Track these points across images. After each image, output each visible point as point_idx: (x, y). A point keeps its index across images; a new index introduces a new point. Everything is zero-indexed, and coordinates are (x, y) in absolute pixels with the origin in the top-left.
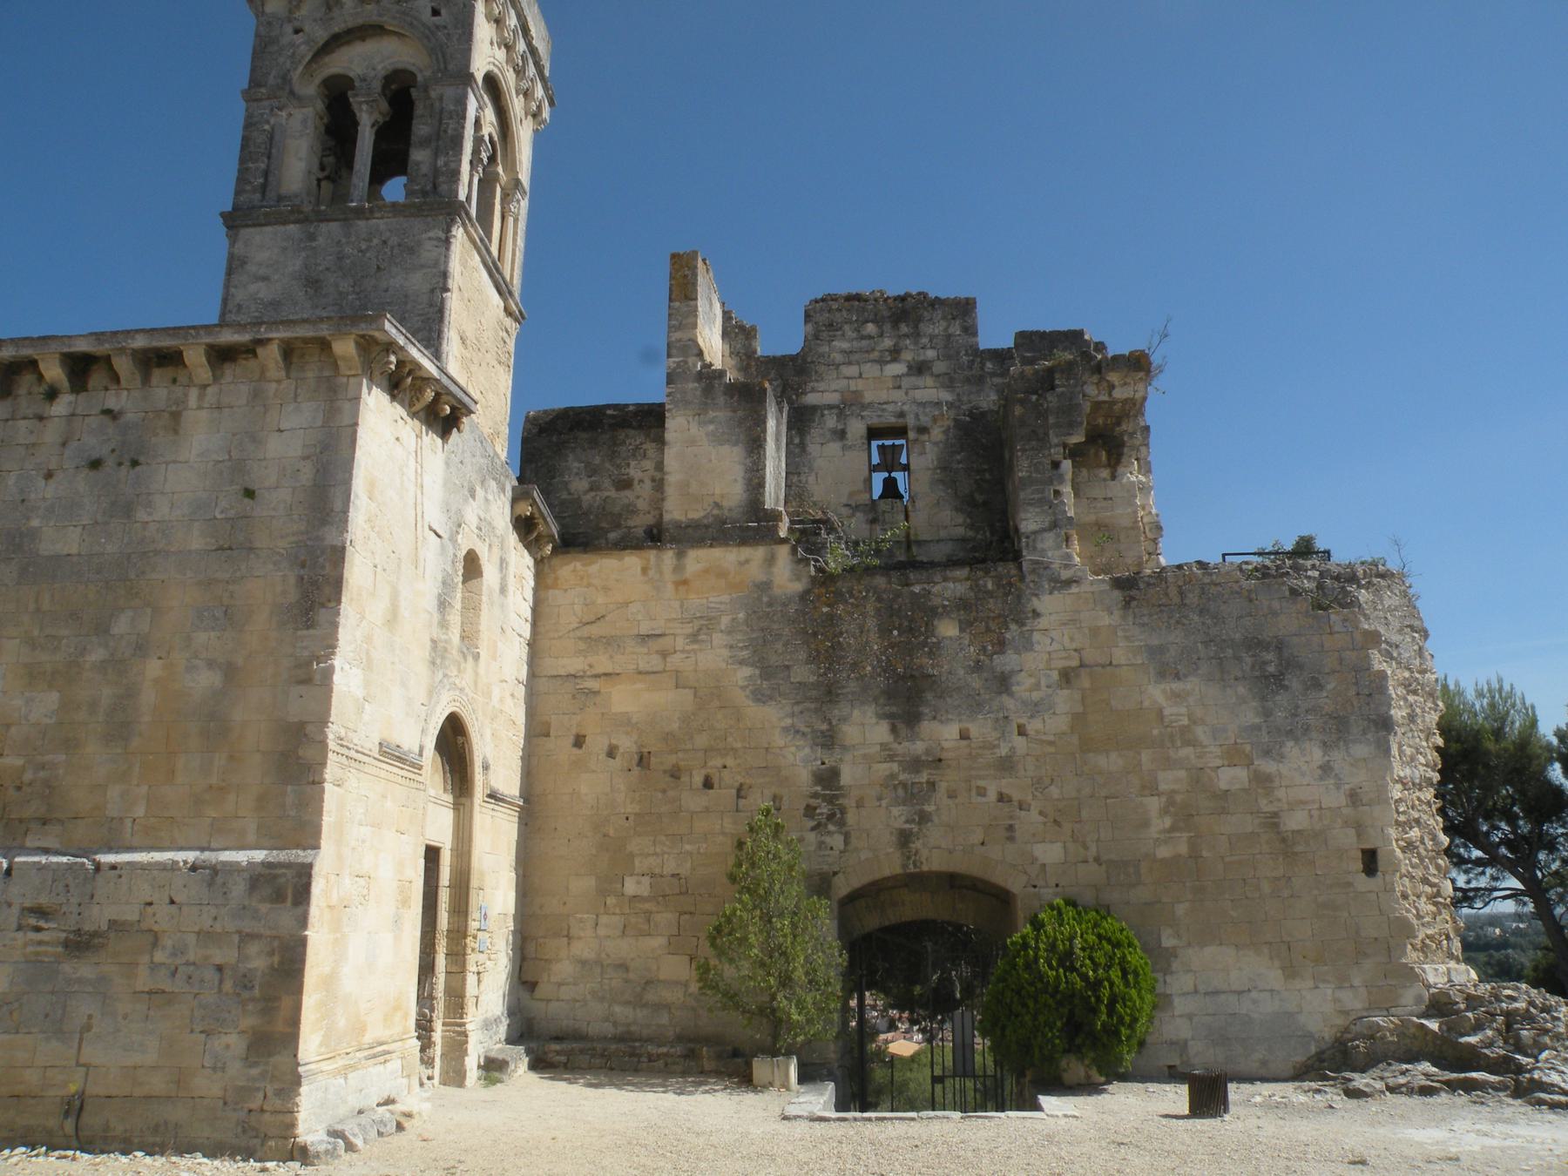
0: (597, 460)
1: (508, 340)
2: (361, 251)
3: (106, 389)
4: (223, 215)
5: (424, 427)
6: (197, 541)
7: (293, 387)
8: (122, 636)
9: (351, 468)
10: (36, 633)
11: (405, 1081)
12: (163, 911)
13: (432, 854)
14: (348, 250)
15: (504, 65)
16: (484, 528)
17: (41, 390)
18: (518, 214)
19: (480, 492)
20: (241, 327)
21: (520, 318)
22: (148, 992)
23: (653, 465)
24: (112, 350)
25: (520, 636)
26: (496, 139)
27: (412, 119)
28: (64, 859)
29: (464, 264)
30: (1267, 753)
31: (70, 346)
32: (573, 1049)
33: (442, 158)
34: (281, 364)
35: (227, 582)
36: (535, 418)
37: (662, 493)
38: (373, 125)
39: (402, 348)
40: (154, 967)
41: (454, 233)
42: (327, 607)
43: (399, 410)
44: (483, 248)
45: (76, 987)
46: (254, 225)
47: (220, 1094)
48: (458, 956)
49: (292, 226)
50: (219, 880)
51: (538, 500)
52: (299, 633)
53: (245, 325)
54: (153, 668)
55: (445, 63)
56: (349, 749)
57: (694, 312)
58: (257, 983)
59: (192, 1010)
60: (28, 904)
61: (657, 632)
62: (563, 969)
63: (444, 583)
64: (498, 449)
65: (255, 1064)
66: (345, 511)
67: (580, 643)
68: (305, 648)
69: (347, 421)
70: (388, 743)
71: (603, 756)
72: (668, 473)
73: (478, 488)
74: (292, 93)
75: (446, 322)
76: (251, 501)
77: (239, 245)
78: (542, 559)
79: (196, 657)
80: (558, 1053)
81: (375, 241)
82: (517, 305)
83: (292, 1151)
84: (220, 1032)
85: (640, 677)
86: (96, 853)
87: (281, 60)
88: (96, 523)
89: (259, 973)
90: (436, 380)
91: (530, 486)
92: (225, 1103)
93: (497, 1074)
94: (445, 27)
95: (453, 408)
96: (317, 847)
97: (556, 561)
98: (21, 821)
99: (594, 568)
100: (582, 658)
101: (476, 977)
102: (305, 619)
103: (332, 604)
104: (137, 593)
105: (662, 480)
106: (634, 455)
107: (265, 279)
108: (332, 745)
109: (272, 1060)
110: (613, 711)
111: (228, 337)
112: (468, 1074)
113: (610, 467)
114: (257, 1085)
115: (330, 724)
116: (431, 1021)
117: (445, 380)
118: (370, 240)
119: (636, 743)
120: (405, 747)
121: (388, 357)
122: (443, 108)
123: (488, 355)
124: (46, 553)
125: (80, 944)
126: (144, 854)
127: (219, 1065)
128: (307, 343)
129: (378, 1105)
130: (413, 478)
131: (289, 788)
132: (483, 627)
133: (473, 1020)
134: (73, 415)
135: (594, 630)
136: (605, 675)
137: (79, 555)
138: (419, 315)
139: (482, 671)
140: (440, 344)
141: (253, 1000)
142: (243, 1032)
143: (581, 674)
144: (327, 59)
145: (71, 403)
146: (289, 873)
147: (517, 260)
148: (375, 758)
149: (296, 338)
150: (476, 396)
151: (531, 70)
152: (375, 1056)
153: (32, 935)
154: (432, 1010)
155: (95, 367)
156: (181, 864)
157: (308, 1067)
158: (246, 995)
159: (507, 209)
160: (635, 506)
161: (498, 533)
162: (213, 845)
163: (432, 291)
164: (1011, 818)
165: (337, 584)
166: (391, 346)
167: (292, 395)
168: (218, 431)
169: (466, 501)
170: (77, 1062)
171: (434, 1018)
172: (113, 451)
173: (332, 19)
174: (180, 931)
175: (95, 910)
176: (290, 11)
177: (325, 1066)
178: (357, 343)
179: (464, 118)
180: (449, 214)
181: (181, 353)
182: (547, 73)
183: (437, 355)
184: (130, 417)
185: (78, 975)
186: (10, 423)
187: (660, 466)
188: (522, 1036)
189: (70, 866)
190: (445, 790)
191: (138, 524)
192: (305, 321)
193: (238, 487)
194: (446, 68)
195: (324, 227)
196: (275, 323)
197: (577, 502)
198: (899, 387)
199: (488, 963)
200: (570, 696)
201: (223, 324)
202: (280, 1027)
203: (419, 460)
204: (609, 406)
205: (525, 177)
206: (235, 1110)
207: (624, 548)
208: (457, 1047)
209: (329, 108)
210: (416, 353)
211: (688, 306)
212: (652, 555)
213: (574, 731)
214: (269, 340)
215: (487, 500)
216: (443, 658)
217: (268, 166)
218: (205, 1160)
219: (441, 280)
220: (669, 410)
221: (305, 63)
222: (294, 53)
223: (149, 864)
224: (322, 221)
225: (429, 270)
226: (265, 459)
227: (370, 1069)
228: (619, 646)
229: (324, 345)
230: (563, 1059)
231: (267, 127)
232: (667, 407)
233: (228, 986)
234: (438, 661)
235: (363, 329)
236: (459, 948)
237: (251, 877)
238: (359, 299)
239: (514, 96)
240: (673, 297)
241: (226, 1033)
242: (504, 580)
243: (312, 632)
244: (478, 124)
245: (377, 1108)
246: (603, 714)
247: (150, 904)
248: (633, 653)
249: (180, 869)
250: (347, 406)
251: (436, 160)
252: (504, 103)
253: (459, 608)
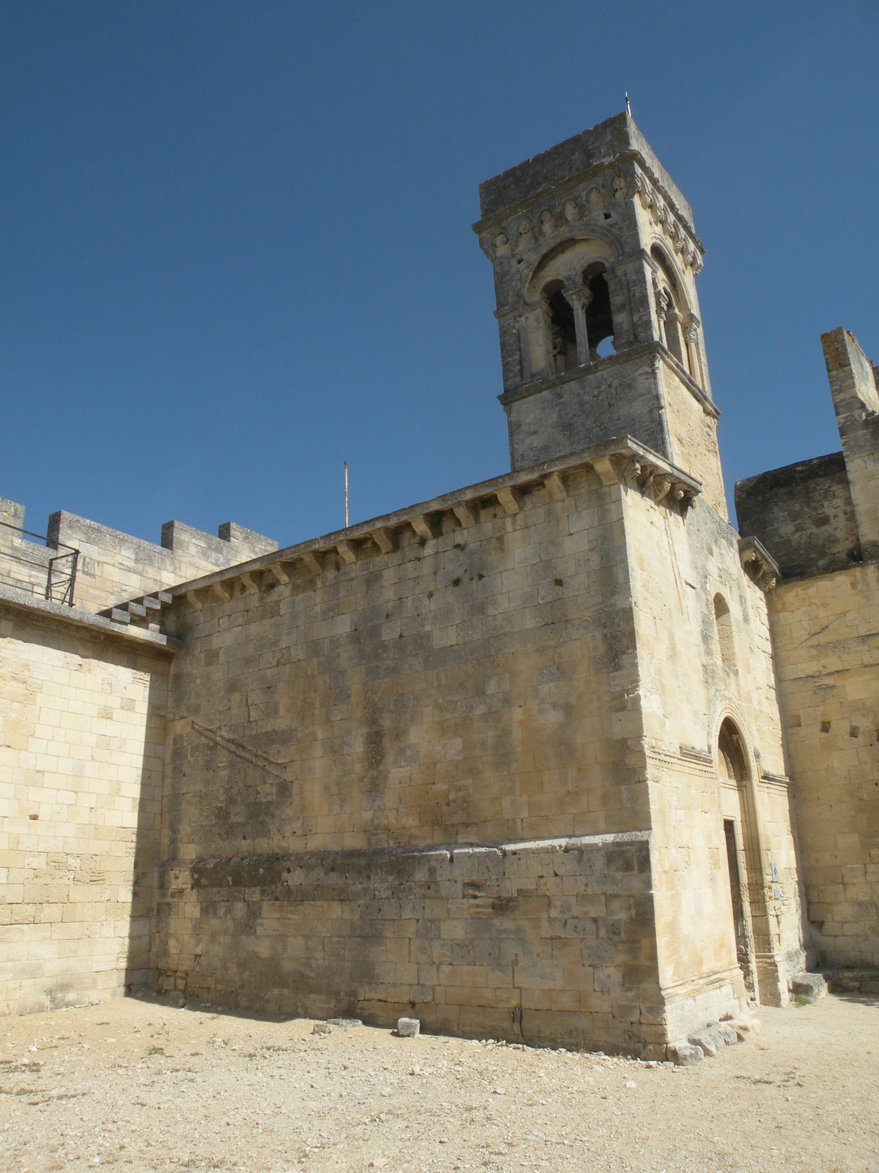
0: (797, 507)
1: (711, 434)
2: (595, 396)
3: (454, 531)
4: (499, 397)
5: (668, 511)
6: (530, 622)
7: (573, 502)
8: (493, 695)
9: (626, 551)
10: (441, 700)
11: (737, 1001)
12: (551, 881)
13: (729, 826)
14: (586, 398)
15: (663, 235)
16: (723, 576)
17: (416, 541)
18: (698, 339)
19: (715, 550)
20: (531, 469)
21: (715, 415)
22: (550, 938)
23: (843, 501)
24: (452, 504)
25: (764, 652)
26: (669, 290)
27: (608, 294)
28: (483, 850)
29: (669, 385)
31: (427, 509)
32: (863, 976)
33: (636, 315)
34: (562, 488)
35: (556, 647)
36: (742, 486)
37: (855, 522)
38: (583, 308)
39: (642, 457)
40: (551, 921)
41: (657, 366)
42: (627, 654)
43: (649, 502)
44: (679, 371)
45: (504, 936)
46: (521, 399)
47: (609, 1010)
48: (759, 902)
49: (545, 392)
50: (585, 857)
51: (759, 547)
52: (611, 675)
53: (534, 467)
54: (517, 714)
55: (622, 249)
56: (660, 754)
57: (850, 375)
58: (622, 930)
59: (581, 951)
60: (466, 881)
61: (874, 632)
62: (844, 910)
63: (703, 622)
64: (721, 515)
65: (630, 989)
66: (627, 581)
67: (812, 650)
68: (616, 685)
69: (615, 518)
70: (686, 747)
71: (847, 736)
72: (857, 505)
73: (713, 547)
74: (525, 303)
75: (666, 431)
76: (561, 588)
77: (514, 414)
78: (770, 590)
79: (544, 703)
80: (851, 979)
81: (603, 387)
82: (711, 405)
83: (666, 1054)
84: (602, 966)
85: (867, 669)
86: (502, 844)
87: (513, 284)
88: (464, 621)
89: (623, 923)
90: (670, 474)
91: (751, 538)
92: (614, 1017)
93: (804, 997)
94: (616, 224)
95: (685, 492)
96: (649, 828)
97: (781, 590)
98: (453, 826)
99: (812, 591)
100: (816, 662)
101: (775, 919)
102: (613, 664)
103: (631, 651)
104: (498, 664)
105: (853, 513)
106: (826, 497)
107: (535, 433)
108: (648, 753)
109: (642, 986)
110: (850, 699)
111: (524, 478)
112: (782, 996)
113: (808, 510)
114: (634, 1004)
115: (644, 738)
116: (746, 954)
117: (676, 473)
118: (599, 387)
119: (872, 722)
120: (698, 748)
121: (634, 465)
122: (628, 280)
123: (700, 448)
124: (438, 647)
125: (502, 906)
126: (532, 843)
127: (605, 989)
128: (576, 470)
129: (721, 1020)
130: (667, 549)
131: (623, 787)
132: (737, 650)
133: (779, 953)
134: (437, 553)
135: (822, 638)
136: (838, 672)
137: (458, 644)
138: (645, 431)
139: (742, 683)
140: (665, 448)
141: (621, 942)
142: (618, 966)
143: (818, 674)
144: (542, 273)
145: (434, 545)
146: (633, 849)
147: (704, 373)
148: (678, 759)
149: (569, 468)
150: (699, 479)
151: (682, 233)
152: (712, 983)
153: (472, 901)
154: (746, 946)
155: (444, 518)
156: (558, 848)
157: (670, 991)
158: (616, 938)
159: (688, 338)
160: (835, 536)
161: (734, 577)
162: (577, 833)
163: (651, 411)
165: (631, 636)
166: (634, 457)
167: (574, 508)
168: (530, 544)
169: (707, 558)
170: (514, 986)
171: (749, 953)
172: (466, 571)
173: (540, 245)
174: (564, 895)
175: (508, 883)
176: (512, 250)
177: (679, 990)
178: (612, 461)
179: (645, 282)
180: (650, 353)
181: (496, 496)
182: (694, 231)
183: (665, 455)
184: (472, 546)
185: (504, 927)
186: (402, 566)
187: (849, 501)
188: (818, 965)
189: (487, 854)
190: (730, 776)
191: (490, 618)
192: (572, 454)
193: (550, 580)
194: (623, 252)
195: (566, 387)
196: (552, 461)
197: (788, 542)
199: (783, 907)
200: (812, 692)
201: (515, 471)
202: (644, 962)
203: (669, 535)
204: (797, 464)
205: (695, 311)
206: (621, 1022)
207: (834, 571)
208: (770, 974)
209: (551, 305)
210: (652, 458)
211: (844, 372)
212: (857, 572)
213: (820, 720)
214: (551, 473)
215: (721, 554)
216: (713, 677)
217: (521, 356)
218: (607, 1057)
219: (655, 401)
220: (847, 456)
221: (529, 281)
222: (520, 277)
223: (537, 849)
224: (563, 383)
225: (645, 397)
226: (565, 556)
227: (711, 993)
228: (843, 647)
229: (588, 468)
230: (856, 984)
231: (514, 331)
232: (845, 454)
233: (602, 932)
234: (710, 680)
235: (614, 450)
236: (760, 897)
237: (606, 854)
238: (601, 430)
239: (675, 255)
240: (830, 368)
241: (606, 967)
242: (745, 612)
243: (619, 673)
244: (655, 284)
245: (720, 1023)
246: (841, 703)
247: (542, 877)
248: (857, 652)
249: (558, 852)
250: (613, 507)
251: (632, 318)
252: (668, 263)
253: (718, 639)
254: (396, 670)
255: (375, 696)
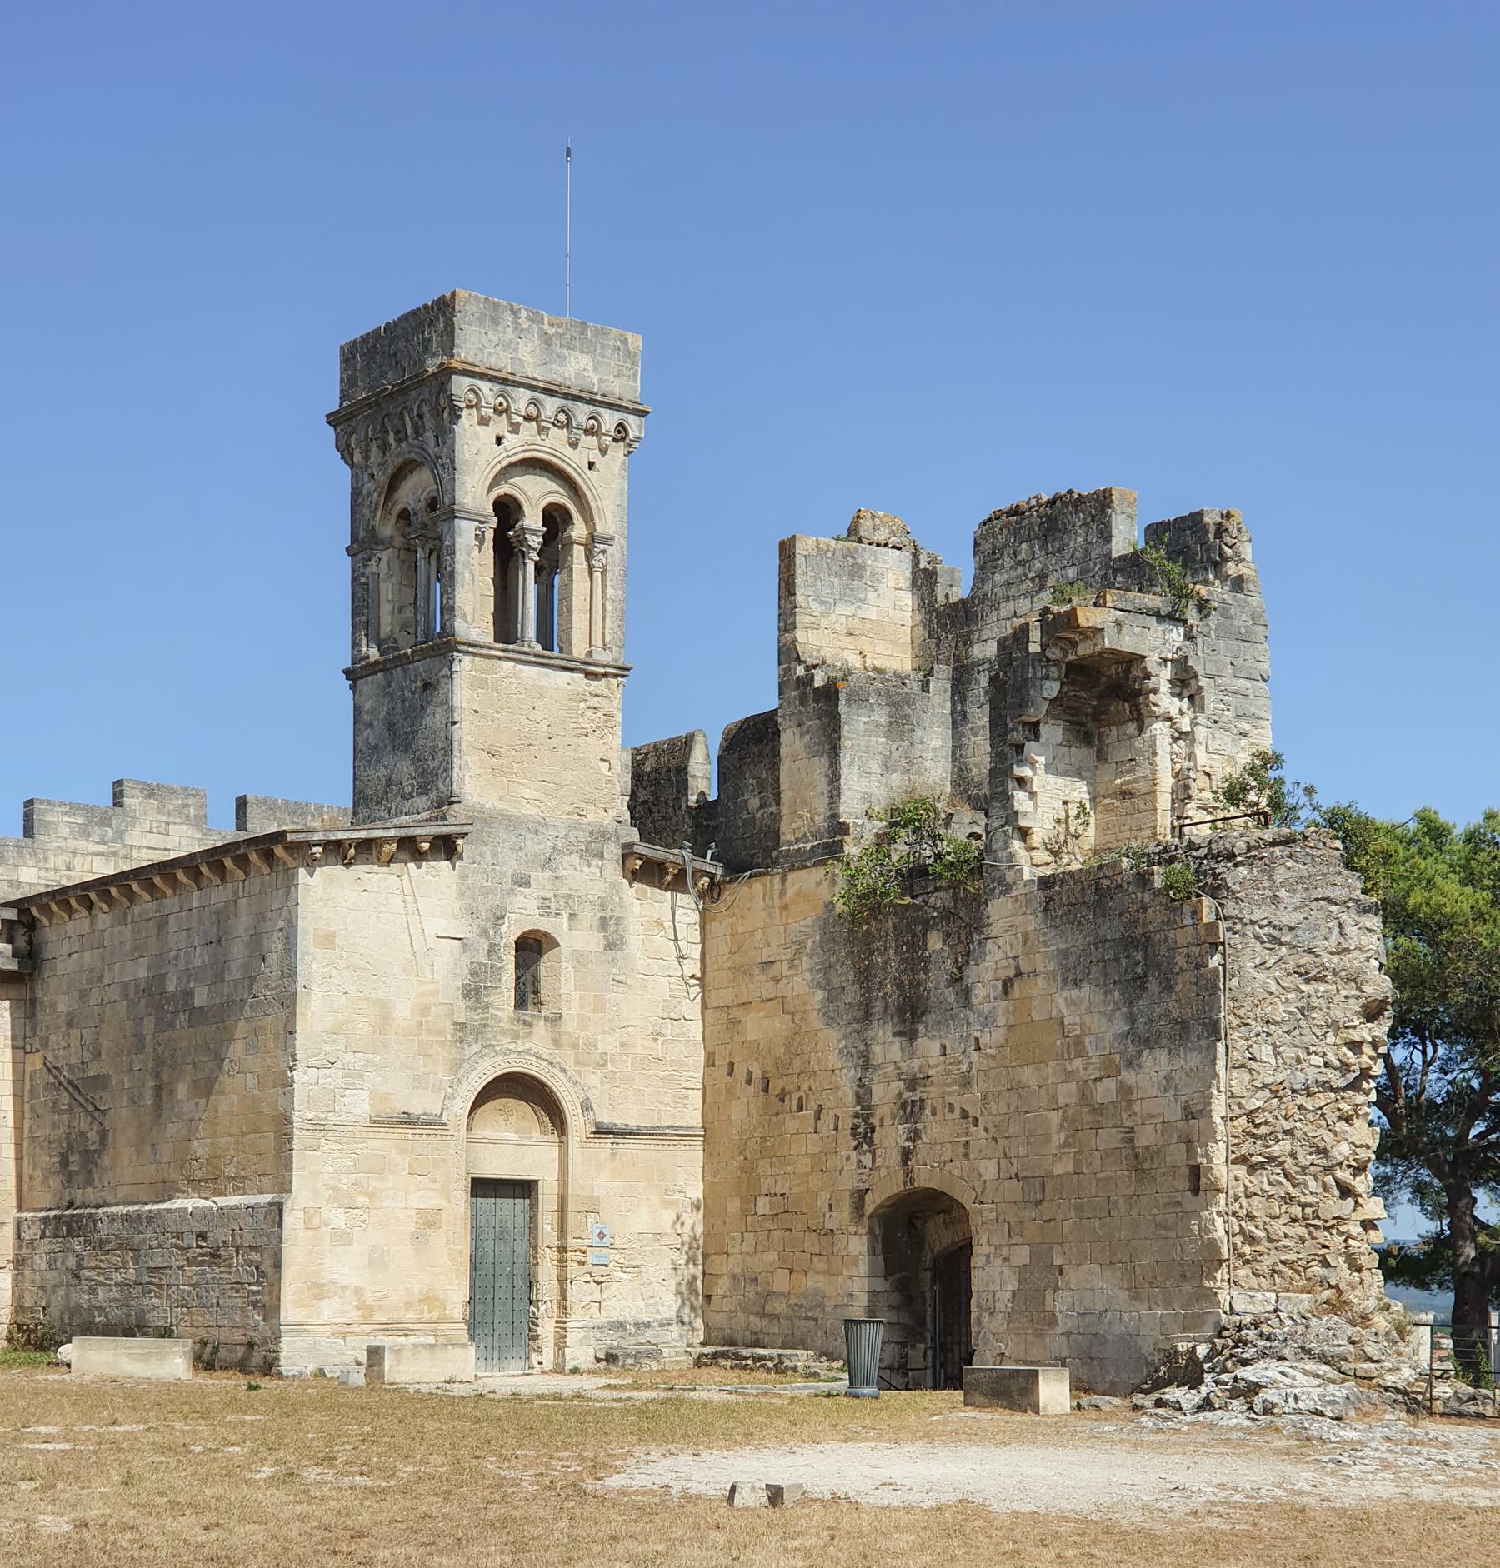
164: (967, 1134)
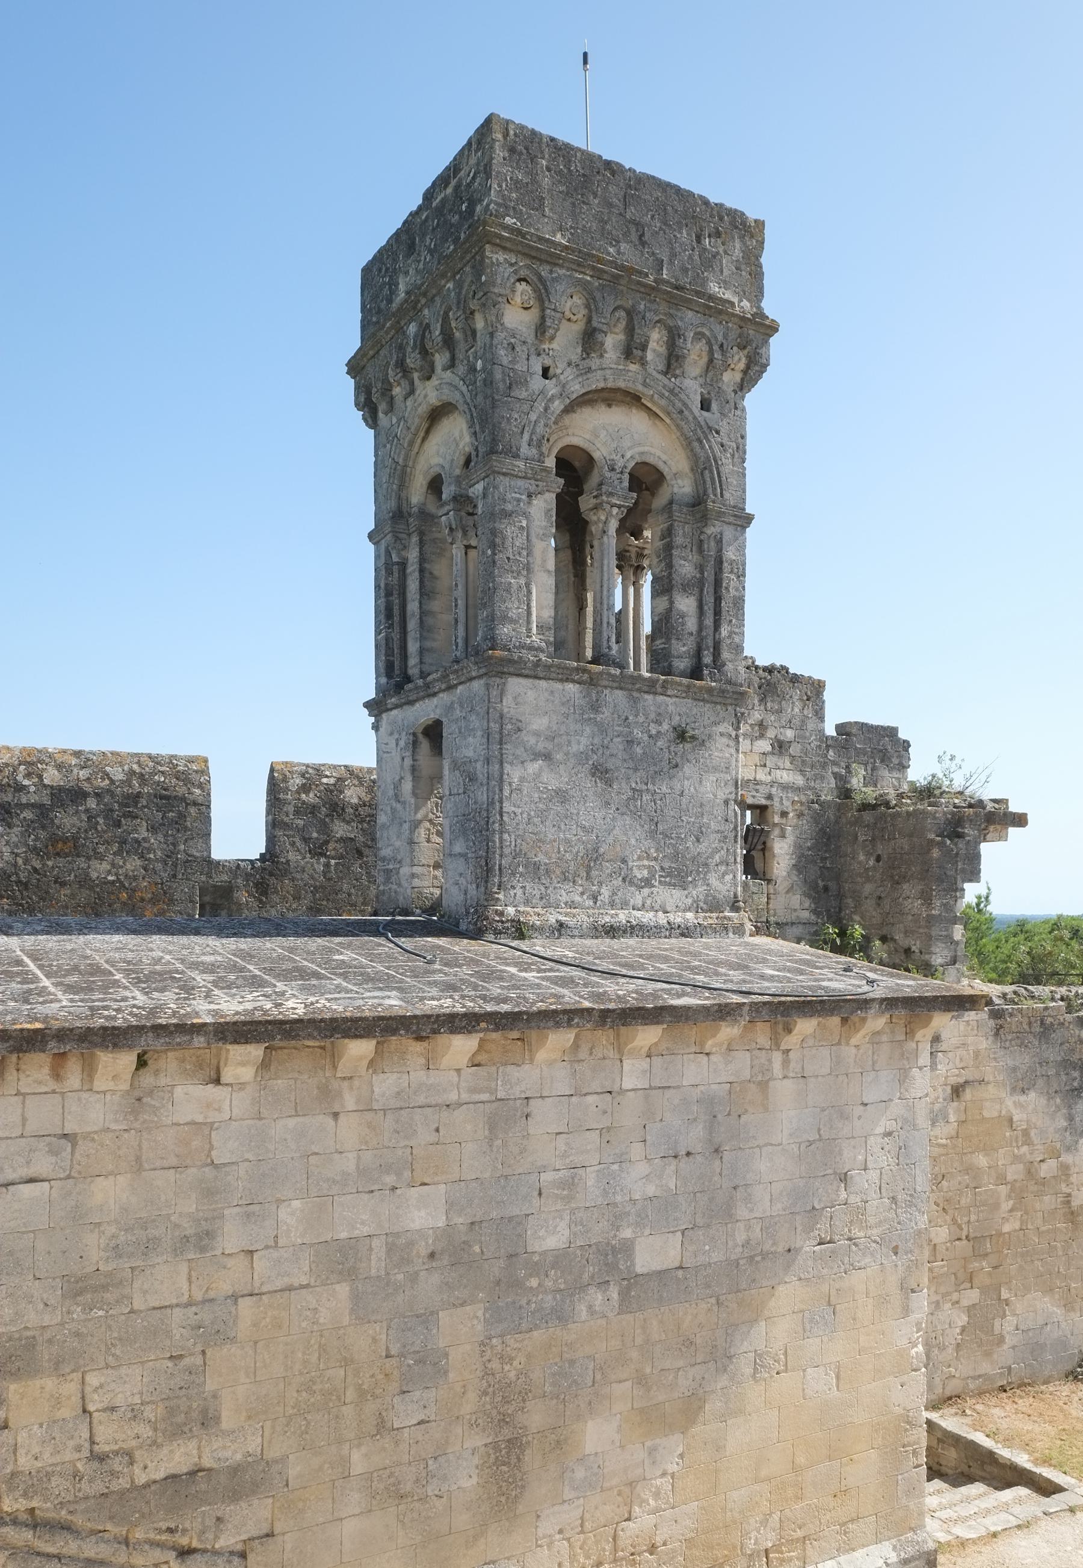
30: (1068, 1149)
49: (571, 685)
198: (765, 766)
254: (561, 1316)
255: (507, 1368)
